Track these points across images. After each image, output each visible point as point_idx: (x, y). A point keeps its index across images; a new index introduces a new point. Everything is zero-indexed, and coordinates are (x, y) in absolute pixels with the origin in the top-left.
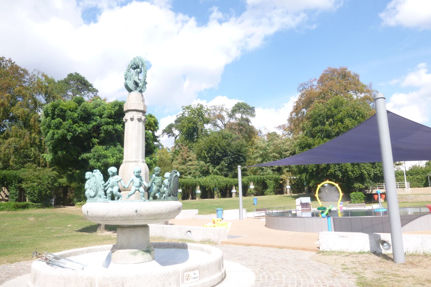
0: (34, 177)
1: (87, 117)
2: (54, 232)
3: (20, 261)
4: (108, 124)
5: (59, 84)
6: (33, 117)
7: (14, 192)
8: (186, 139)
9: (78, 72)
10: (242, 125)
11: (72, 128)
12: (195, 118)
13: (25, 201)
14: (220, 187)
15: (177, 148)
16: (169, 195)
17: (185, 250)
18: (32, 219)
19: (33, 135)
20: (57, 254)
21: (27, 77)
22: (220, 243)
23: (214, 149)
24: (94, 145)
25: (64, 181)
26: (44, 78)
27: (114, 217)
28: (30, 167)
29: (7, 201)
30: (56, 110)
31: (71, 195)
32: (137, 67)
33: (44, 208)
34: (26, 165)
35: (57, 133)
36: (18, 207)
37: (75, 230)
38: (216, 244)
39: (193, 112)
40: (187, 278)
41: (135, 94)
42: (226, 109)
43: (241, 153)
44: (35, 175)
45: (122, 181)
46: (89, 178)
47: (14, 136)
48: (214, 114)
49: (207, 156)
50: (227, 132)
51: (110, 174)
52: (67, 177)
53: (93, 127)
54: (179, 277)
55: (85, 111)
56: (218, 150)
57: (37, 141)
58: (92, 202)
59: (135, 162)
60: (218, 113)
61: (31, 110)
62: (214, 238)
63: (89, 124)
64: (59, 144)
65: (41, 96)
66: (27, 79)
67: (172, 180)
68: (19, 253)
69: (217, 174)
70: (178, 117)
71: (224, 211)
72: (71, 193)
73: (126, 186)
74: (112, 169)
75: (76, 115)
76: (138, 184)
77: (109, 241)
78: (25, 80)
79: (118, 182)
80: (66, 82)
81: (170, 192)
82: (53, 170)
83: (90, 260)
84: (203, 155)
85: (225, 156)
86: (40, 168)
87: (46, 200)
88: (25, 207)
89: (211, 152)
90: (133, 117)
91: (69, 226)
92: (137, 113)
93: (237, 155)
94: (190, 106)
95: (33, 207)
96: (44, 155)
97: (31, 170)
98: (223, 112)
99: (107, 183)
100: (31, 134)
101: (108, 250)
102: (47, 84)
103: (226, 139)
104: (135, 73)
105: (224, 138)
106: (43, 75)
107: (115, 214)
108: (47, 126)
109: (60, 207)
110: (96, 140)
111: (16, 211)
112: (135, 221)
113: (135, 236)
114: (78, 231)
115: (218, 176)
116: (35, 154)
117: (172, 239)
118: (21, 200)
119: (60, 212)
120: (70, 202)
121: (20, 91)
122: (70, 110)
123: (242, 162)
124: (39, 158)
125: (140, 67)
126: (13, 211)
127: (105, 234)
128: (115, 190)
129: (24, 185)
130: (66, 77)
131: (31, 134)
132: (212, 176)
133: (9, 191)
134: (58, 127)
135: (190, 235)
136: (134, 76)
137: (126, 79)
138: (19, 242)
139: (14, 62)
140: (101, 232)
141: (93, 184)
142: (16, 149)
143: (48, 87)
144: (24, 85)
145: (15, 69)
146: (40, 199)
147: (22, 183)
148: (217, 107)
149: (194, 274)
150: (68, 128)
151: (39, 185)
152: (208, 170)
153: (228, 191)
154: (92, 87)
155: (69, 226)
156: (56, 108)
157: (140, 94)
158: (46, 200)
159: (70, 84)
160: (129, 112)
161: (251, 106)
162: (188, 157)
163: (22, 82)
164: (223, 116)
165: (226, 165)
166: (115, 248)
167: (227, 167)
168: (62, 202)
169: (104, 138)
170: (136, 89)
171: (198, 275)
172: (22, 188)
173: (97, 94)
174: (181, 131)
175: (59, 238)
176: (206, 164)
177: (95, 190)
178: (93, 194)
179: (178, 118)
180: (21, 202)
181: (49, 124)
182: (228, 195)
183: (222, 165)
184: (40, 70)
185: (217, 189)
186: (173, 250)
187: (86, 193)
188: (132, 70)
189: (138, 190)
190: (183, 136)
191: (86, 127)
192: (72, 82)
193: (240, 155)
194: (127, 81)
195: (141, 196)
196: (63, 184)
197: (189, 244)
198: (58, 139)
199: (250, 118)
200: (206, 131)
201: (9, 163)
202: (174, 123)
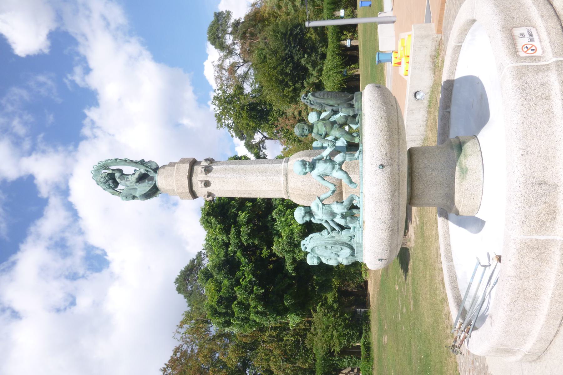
0: (326, 336)
1: (229, 265)
2: (407, 310)
3: (456, 363)
4: (238, 233)
5: (193, 306)
6: (240, 339)
7: (346, 361)
8: (267, 121)
9: (174, 280)
10: (245, 33)
11: (246, 286)
12: (234, 108)
13: (359, 346)
14: (341, 65)
15: (282, 134)
16: (352, 106)
17: (456, 85)
18: (385, 339)
19: (265, 338)
20: (454, 313)
21: (185, 347)
22: (439, 36)
23: (281, 76)
24: (273, 255)
25: (330, 297)
26: (185, 326)
27: (393, 210)
28: (311, 340)
29: (359, 370)
30: (219, 310)
31: (352, 285)
32: (111, 177)
33: (370, 321)
34: (308, 346)
35: (255, 307)
36: (368, 357)
37: (404, 280)
38: (440, 43)
39: (225, 111)
40: (530, 52)
41: (160, 180)
42: (220, 60)
43: (287, 32)
44: (322, 334)
45: (322, 197)
46: (319, 258)
47: (268, 362)
48: (227, 79)
49: (292, 87)
50: (255, 56)
51: (307, 219)
52: (326, 292)
53: (244, 256)
54: (528, 66)
55: (219, 267)
56: (282, 70)
57: (274, 333)
58: (362, 251)
59: (286, 175)
60: (227, 74)
61: (231, 341)
62: (429, 47)
63: (239, 263)
64: (272, 304)
65: (211, 329)
66: (188, 347)
67: (322, 101)
68: (441, 362)
69: (321, 70)
70: (234, 134)
71: (380, 49)
72: (349, 285)
73: (332, 188)
74: (299, 216)
75: (226, 282)
76: (328, 166)
77: (425, 228)
78: (189, 350)
79: (323, 205)
80: (189, 296)
81: (345, 105)
82: (315, 311)
83: (467, 255)
84: (291, 94)
85: (292, 58)
86: (313, 328)
87: (358, 319)
88: (368, 347)
89: (286, 80)
90: (201, 181)
91: (397, 288)
92: (194, 174)
93: (291, 39)
94: (216, 116)
95: (367, 336)
96: (292, 327)
97: (315, 339)
98: (224, 65)
99: (325, 225)
100: (264, 342)
101: (447, 225)
102: (193, 321)
103: (265, 57)
104: (123, 182)
105: (264, 60)
106: (181, 326)
107: (387, 207)
108: (246, 323)
109: (369, 299)
110: (265, 252)
111: (373, 359)
112: (401, 169)
113: (430, 171)
114: (406, 276)
115: (324, 68)
116: (292, 335)
117: (426, 125)
118: (358, 353)
119: (376, 300)
120: (361, 287)
121: (205, 356)
122: (219, 291)
123: (301, 30)
124: (299, 329)
125: (110, 172)
126: (373, 362)
127: (413, 235)
128: (339, 209)
129: (337, 349)
130: (181, 296)
131: (264, 342)
132: (324, 78)
133: (345, 368)
134: (245, 307)
135: (422, 94)
136: (128, 183)
137: (134, 197)
138: (420, 359)
139: (166, 364)
140: (410, 241)
141: (329, 251)
142: (287, 360)
143: (197, 320)
144: (196, 351)
145: (173, 363)
146: (356, 327)
147: (334, 351)
148: (217, 75)
149: (522, 36)
150: (246, 293)
151: (337, 329)
152: (314, 84)
153: (349, 53)
154: (194, 260)
155: (397, 288)
156: (216, 310)
157: (160, 171)
158: (358, 319)
159: (192, 290)
160: (194, 189)
161: (212, 18)
162: (295, 117)
163: (193, 354)
164: (230, 66)
165: (306, 56)
166: (447, 210)
167: (310, 55)
168: (362, 298)
169: (261, 239)
170: (152, 179)
171: (524, 30)
172: (341, 351)
173: (204, 254)
174: (255, 130)
175: (416, 302)
176: (304, 88)
177: (339, 247)
178: (347, 251)
179: (237, 135)
180: (360, 352)
181: (242, 320)
182: (354, 53)
183: (307, 63)
184: (174, 331)
185: (345, 70)
186: (454, 109)
187: (345, 262)
188: (120, 187)
189: (340, 164)
190: (262, 126)
191: (244, 266)
192: (189, 287)
193: (291, 34)
194: (137, 194)
195: (351, 160)
196: (335, 297)
197: (444, 78)
198: (265, 306)
199: (232, 21)
200: (254, 91)
201: (305, 369)
202: (244, 141)
